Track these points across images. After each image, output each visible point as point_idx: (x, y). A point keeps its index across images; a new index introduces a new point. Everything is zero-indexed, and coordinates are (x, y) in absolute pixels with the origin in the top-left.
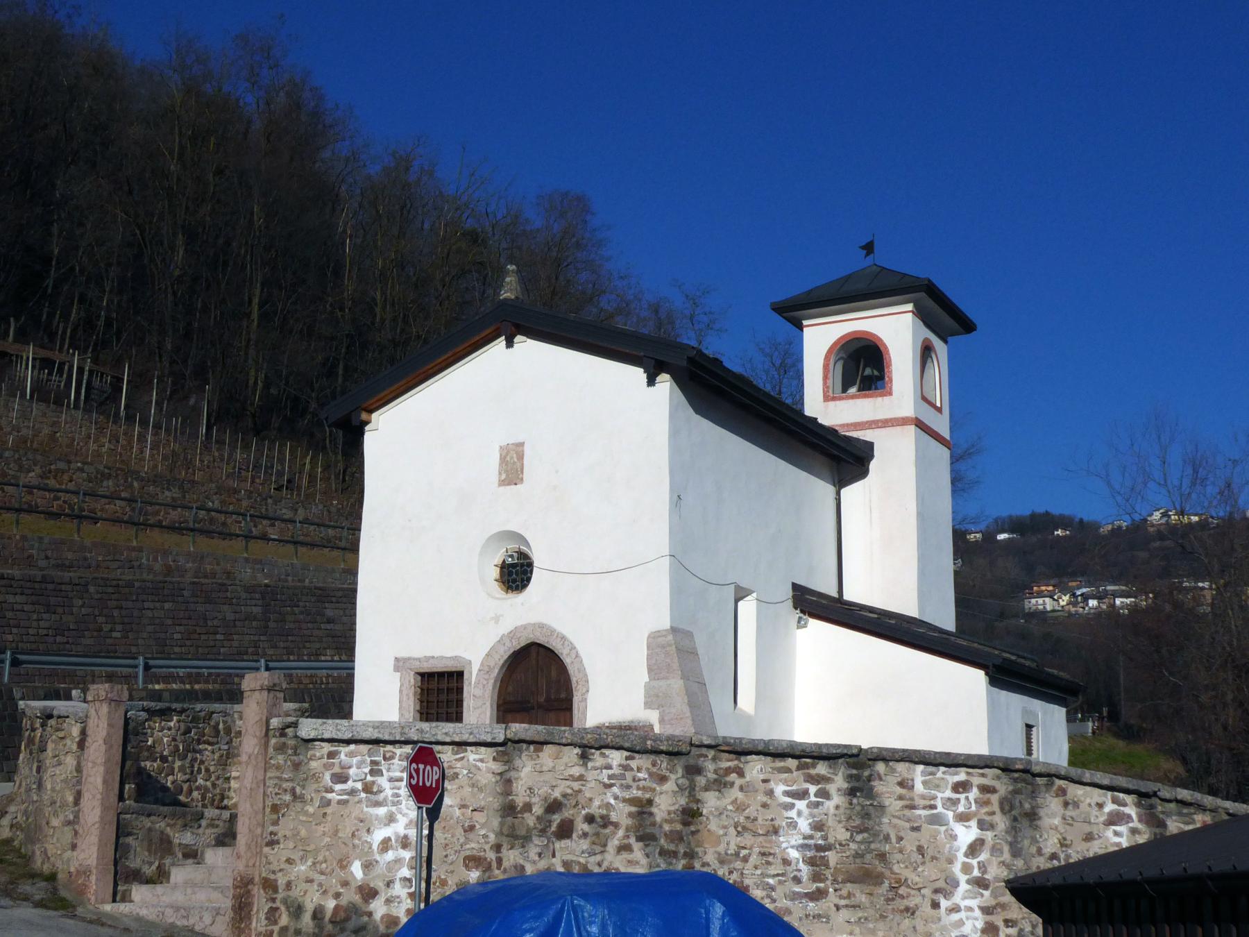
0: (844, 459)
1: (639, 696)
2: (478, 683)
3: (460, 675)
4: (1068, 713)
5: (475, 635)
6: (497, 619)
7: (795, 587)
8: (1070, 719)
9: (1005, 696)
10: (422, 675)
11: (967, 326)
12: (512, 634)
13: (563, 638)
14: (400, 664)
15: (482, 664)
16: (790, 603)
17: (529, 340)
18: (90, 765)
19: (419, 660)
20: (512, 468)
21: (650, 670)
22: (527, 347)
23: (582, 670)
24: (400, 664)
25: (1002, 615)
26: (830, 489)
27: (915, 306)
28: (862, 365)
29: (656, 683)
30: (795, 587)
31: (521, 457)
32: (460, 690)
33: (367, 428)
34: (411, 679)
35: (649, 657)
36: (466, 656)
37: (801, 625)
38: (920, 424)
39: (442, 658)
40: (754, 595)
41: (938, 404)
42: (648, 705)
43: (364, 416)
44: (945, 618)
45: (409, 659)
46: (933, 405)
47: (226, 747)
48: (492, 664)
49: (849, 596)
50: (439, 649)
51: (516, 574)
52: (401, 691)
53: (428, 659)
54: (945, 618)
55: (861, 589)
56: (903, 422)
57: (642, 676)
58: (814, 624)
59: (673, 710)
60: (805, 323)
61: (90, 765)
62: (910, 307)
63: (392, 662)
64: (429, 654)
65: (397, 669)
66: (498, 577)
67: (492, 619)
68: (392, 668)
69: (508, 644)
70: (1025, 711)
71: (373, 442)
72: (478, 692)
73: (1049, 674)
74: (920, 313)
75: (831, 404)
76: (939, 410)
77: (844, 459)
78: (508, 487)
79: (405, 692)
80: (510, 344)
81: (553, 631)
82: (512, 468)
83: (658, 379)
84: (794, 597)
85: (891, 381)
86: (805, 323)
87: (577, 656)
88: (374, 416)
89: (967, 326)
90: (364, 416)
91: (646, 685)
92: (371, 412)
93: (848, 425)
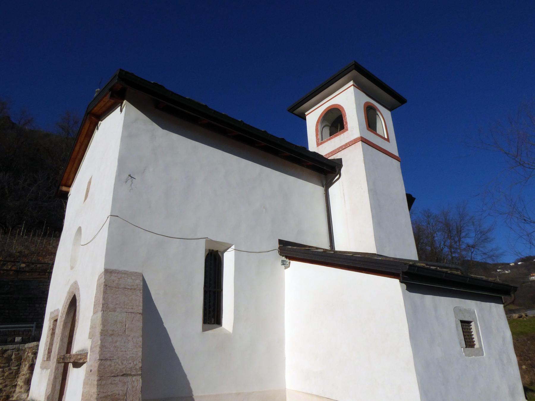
0: (326, 171)
4: (504, 307)
7: (281, 242)
8: (508, 312)
9: (417, 296)
11: (402, 101)
16: (276, 253)
25: (524, 283)
26: (319, 190)
27: (354, 81)
28: (335, 122)
30: (281, 242)
37: (287, 267)
38: (364, 140)
40: (233, 247)
41: (386, 137)
43: (64, 189)
44: (408, 251)
46: (384, 138)
47: (16, 368)
49: (337, 249)
54: (408, 251)
55: (343, 244)
56: (354, 142)
58: (294, 264)
60: (306, 114)
62: (351, 83)
70: (457, 310)
73: (472, 278)
74: (359, 86)
75: (320, 146)
76: (388, 140)
77: (326, 171)
84: (279, 248)
85: (347, 123)
86: (306, 114)
89: (402, 101)
90: (64, 189)
93: (328, 154)
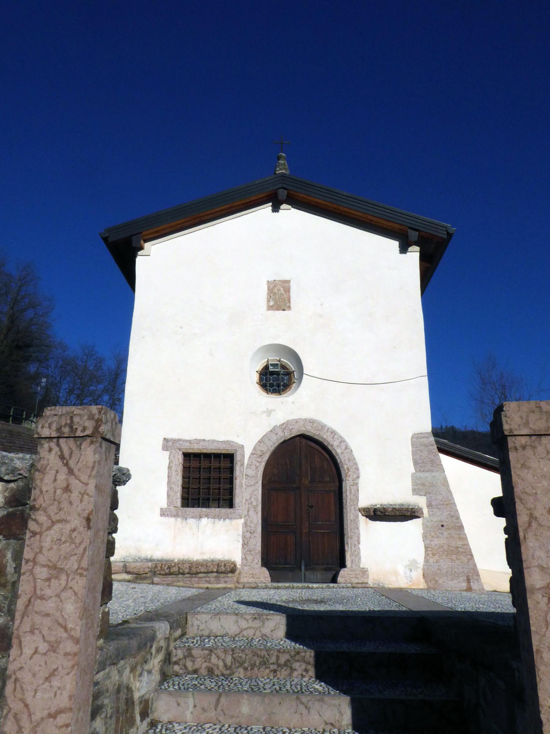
1: (408, 484)
2: (250, 465)
3: (229, 458)
5: (248, 425)
6: (269, 413)
10: (187, 456)
12: (284, 426)
13: (333, 433)
14: (168, 444)
15: (255, 449)
17: (292, 209)
18: (42, 573)
19: (190, 441)
20: (279, 297)
21: (416, 463)
22: (290, 215)
23: (352, 459)
24: (168, 444)
29: (422, 475)
31: (288, 290)
32: (231, 470)
33: (139, 253)
34: (180, 458)
35: (414, 453)
36: (239, 441)
39: (214, 441)
42: (416, 491)
45: (179, 440)
48: (265, 449)
50: (210, 432)
51: (277, 378)
52: (170, 468)
53: (198, 441)
57: (411, 468)
59: (440, 497)
61: (42, 573)
63: (161, 443)
64: (199, 437)
65: (165, 448)
66: (258, 381)
67: (264, 412)
68: (160, 447)
69: (280, 434)
71: (142, 263)
72: (251, 472)
78: (277, 312)
79: (174, 468)
80: (276, 209)
81: (323, 426)
82: (279, 297)
83: (410, 249)
87: (347, 447)
88: (147, 245)
91: (413, 475)
92: (146, 241)
